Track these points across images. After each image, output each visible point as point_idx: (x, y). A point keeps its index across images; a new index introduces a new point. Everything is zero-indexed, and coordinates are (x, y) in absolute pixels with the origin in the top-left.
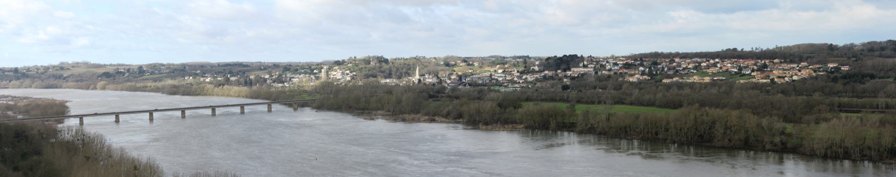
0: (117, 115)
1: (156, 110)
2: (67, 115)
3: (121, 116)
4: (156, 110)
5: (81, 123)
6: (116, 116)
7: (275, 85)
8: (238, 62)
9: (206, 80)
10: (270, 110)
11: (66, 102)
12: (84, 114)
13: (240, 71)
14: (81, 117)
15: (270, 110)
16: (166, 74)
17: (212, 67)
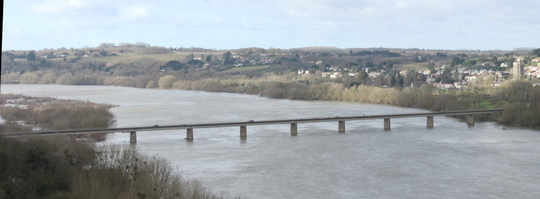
0: (190, 129)
1: (252, 123)
2: (111, 127)
3: (195, 131)
4: (252, 123)
5: (133, 141)
6: (188, 130)
7: (440, 85)
8: (382, 48)
9: (331, 76)
10: (430, 126)
11: (110, 106)
12: (137, 125)
13: (385, 63)
14: (133, 131)
15: (430, 126)
16: (269, 66)
17: (340, 55)
